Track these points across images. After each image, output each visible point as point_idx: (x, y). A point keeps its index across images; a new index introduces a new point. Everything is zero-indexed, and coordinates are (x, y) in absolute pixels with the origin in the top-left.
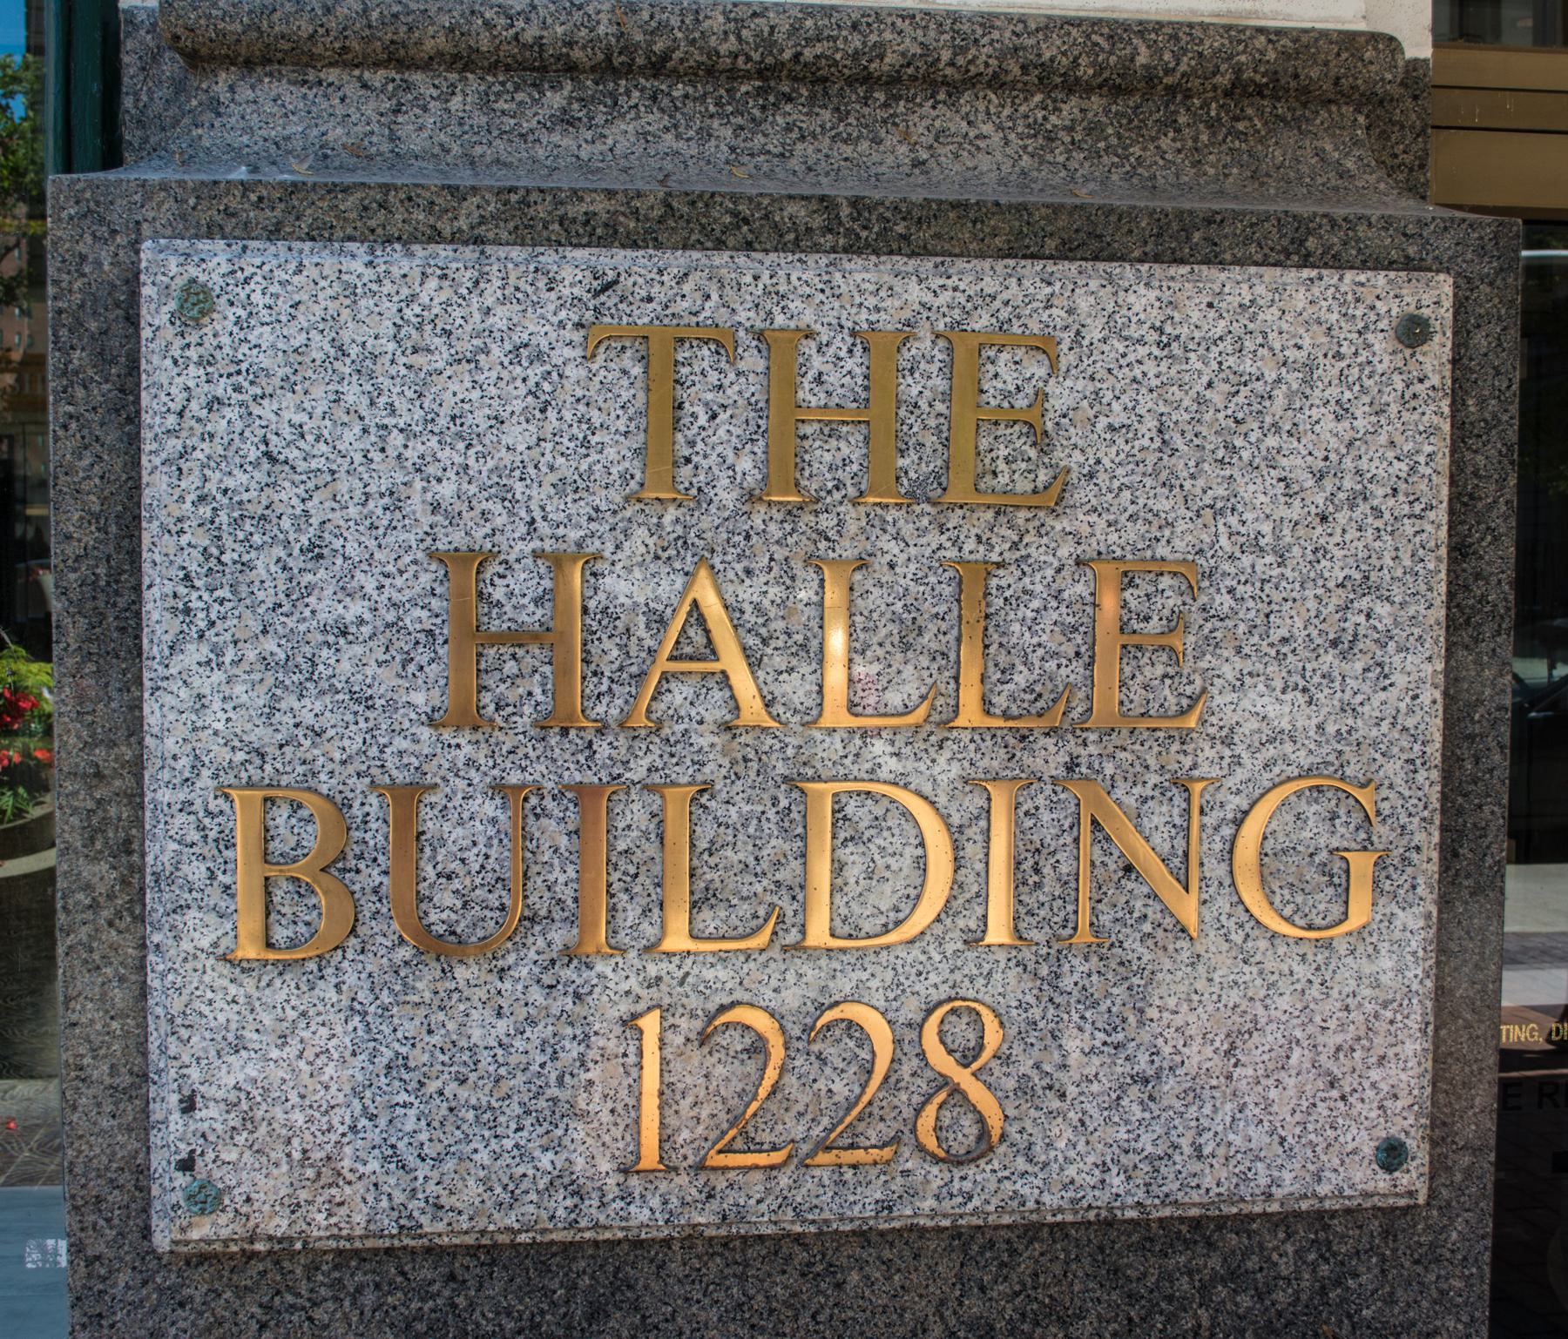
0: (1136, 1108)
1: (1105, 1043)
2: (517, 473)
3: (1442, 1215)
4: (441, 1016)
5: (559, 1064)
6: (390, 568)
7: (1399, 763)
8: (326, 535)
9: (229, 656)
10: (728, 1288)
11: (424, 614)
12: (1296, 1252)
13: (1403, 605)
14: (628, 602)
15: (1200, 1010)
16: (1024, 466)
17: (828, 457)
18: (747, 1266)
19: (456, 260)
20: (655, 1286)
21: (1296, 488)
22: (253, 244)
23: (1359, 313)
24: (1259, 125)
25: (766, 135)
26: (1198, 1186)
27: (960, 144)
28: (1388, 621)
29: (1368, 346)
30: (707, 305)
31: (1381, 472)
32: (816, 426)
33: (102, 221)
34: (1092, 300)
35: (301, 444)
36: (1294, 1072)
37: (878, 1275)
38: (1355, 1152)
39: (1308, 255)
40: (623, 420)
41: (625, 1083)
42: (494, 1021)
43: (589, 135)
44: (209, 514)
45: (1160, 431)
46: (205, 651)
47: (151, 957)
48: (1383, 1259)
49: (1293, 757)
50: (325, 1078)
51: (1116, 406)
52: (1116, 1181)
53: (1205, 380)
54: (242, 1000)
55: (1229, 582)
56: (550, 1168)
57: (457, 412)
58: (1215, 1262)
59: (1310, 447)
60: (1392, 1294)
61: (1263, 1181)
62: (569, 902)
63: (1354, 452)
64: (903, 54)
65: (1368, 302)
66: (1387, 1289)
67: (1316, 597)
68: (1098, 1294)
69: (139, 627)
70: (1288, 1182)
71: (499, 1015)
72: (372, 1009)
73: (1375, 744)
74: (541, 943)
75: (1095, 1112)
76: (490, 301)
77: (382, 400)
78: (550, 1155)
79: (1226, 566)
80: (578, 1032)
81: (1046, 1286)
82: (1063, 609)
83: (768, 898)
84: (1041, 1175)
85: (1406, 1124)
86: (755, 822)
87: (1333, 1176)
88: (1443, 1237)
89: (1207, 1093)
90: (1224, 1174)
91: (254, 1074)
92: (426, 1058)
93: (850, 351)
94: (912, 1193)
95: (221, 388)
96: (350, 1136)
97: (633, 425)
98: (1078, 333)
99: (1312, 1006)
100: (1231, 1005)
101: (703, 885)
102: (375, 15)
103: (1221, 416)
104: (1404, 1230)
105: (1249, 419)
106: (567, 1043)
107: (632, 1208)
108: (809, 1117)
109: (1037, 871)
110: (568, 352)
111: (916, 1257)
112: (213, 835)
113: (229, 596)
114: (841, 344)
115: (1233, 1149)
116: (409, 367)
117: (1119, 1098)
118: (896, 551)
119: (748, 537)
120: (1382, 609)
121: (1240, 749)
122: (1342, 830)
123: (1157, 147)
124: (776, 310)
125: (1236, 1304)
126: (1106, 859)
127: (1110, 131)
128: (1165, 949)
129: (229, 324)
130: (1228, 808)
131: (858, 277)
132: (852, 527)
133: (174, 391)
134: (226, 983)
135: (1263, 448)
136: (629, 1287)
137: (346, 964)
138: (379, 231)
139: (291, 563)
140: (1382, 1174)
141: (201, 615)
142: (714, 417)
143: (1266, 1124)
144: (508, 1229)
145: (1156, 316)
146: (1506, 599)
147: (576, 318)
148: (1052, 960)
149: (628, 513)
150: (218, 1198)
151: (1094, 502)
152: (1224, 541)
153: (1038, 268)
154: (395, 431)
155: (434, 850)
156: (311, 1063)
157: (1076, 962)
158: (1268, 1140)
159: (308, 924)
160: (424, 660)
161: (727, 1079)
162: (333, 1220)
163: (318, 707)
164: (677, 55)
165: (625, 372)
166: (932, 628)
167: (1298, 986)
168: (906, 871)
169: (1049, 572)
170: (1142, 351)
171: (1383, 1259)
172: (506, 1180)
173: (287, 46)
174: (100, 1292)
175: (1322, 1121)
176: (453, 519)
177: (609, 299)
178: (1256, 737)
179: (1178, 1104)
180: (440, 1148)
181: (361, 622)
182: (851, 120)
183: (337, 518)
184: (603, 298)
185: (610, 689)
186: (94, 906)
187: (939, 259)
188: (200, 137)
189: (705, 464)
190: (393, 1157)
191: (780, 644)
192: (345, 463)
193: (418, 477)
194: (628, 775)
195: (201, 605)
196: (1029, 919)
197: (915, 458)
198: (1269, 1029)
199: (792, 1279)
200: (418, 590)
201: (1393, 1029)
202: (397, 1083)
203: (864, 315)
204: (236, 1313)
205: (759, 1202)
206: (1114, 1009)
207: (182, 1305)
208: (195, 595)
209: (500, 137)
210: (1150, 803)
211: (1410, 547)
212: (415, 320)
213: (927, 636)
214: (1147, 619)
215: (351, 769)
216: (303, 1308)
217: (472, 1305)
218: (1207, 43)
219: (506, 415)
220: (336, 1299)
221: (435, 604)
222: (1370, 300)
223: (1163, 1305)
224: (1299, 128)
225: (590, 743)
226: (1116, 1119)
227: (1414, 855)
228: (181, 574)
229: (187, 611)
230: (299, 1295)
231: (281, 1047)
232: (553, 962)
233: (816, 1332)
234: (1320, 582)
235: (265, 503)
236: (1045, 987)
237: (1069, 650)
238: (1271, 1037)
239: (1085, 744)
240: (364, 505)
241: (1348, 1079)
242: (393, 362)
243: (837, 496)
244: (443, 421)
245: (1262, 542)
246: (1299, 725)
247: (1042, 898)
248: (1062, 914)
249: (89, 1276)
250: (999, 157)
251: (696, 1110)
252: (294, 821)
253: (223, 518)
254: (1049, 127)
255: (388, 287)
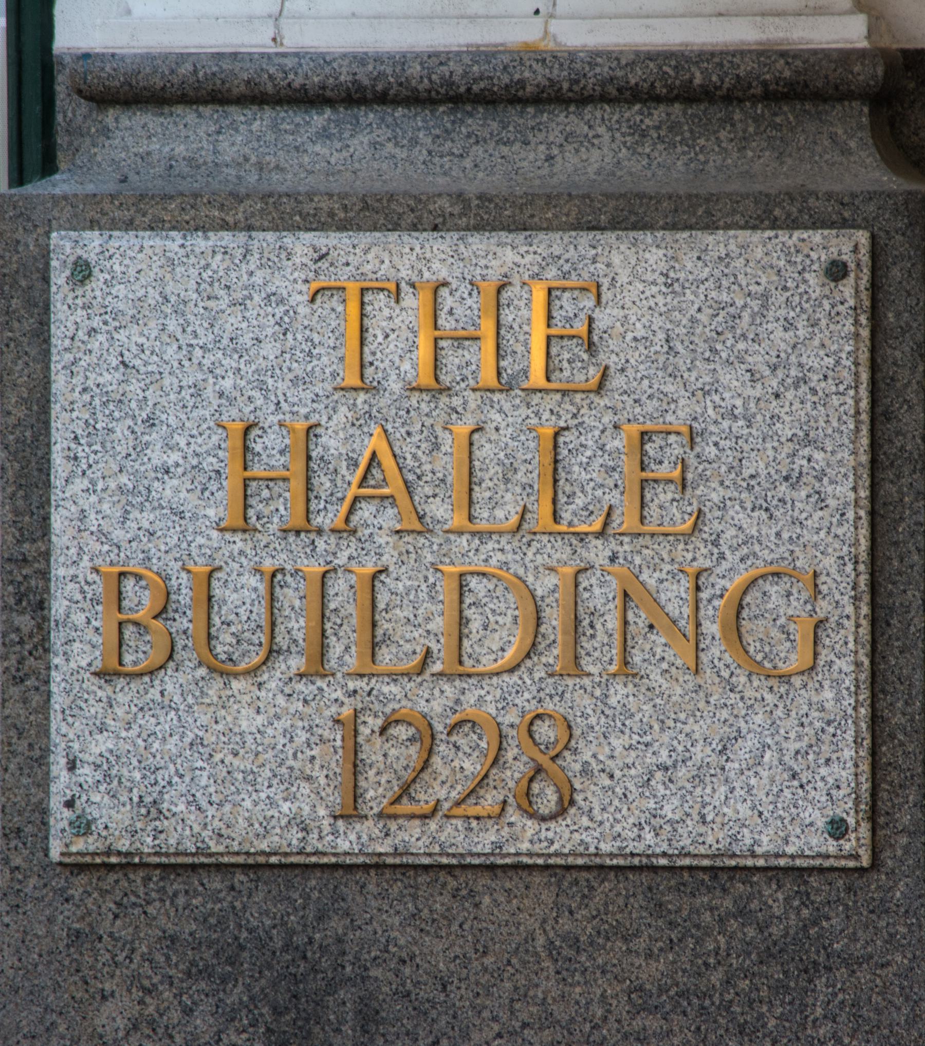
0: (661, 787)
1: (639, 743)
2: (269, 373)
3: (888, 879)
4: (223, 712)
5: (294, 745)
6: (195, 432)
7: (833, 559)
8: (157, 412)
9: (100, 486)
10: (406, 903)
11: (214, 460)
12: (785, 899)
13: (833, 453)
14: (336, 453)
15: (702, 722)
16: (580, 364)
17: (457, 361)
18: (418, 889)
19: (233, 242)
20: (359, 899)
21: (758, 376)
22: (116, 233)
23: (799, 260)
24: (791, 118)
25: (453, 141)
26: (704, 843)
27: (581, 142)
28: (823, 464)
29: (805, 281)
30: (383, 267)
31: (816, 365)
32: (450, 342)
33: (29, 219)
34: (622, 257)
35: (142, 356)
36: (767, 767)
37: (503, 899)
38: (811, 824)
39: (776, 219)
40: (333, 339)
41: (334, 759)
42: (255, 716)
43: (338, 145)
44: (89, 399)
45: (667, 341)
46: (86, 483)
47: (53, 673)
48: (847, 907)
49: (760, 554)
50: (153, 750)
51: (638, 325)
52: (649, 837)
53: (696, 306)
54: (104, 699)
55: (714, 438)
56: (288, 812)
57: (233, 336)
58: (728, 903)
59: (767, 349)
60: (854, 933)
61: (748, 841)
62: (301, 641)
63: (797, 352)
64: (538, 86)
65: (805, 252)
66: (851, 930)
67: (773, 448)
68: (649, 920)
69: (49, 468)
70: (765, 843)
71: (258, 712)
72: (182, 707)
73: (816, 545)
74: (283, 667)
75: (633, 789)
76: (252, 267)
77: (189, 329)
78: (288, 804)
79: (712, 428)
80: (306, 725)
81: (614, 914)
82: (606, 457)
83: (422, 641)
84: (598, 830)
85: (847, 807)
86: (413, 592)
87: (796, 840)
88: (890, 894)
89: (708, 779)
90: (721, 836)
91: (111, 747)
92: (213, 739)
93: (470, 294)
94: (515, 839)
95: (96, 322)
96: (168, 788)
97: (338, 343)
98: (613, 279)
99: (778, 722)
100: (722, 719)
101: (382, 632)
102: (201, 74)
103: (707, 330)
104: (861, 889)
105: (726, 332)
106: (299, 732)
107: (339, 840)
108: (448, 784)
109: (592, 626)
110: (299, 298)
111: (527, 888)
112: (89, 596)
113: (99, 449)
114: (464, 289)
115: (726, 819)
116: (205, 308)
117: (649, 780)
118: (500, 420)
119: (408, 412)
120: (818, 456)
121: (724, 548)
122: (795, 603)
123: (717, 138)
124: (424, 269)
125: (744, 934)
126: (637, 620)
127: (686, 128)
128: (677, 680)
129: (101, 284)
130: (717, 587)
131: (474, 247)
132: (472, 405)
133: (69, 324)
134: (95, 688)
135: (735, 350)
136: (343, 900)
137: (167, 678)
138: (192, 222)
139: (136, 429)
140: (831, 841)
141: (84, 461)
142: (387, 336)
143: (749, 802)
144: (263, 853)
145: (663, 266)
146: (919, 449)
147: (303, 277)
148: (603, 686)
149: (336, 397)
150: (89, 824)
151: (625, 387)
152: (710, 411)
153: (591, 237)
154: (197, 348)
155: (220, 607)
156: (145, 741)
157: (619, 687)
158: (750, 813)
159: (144, 652)
160: (214, 489)
161: (398, 758)
162: (157, 842)
163: (152, 517)
164: (392, 92)
165: (333, 310)
166: (523, 469)
167: (768, 709)
168: (508, 625)
169: (597, 433)
170: (654, 289)
171: (847, 907)
172: (261, 819)
173: (148, 94)
174: (18, 890)
175: (787, 802)
176: (232, 401)
177: (324, 264)
178: (735, 541)
179: (689, 786)
180: (221, 797)
181: (177, 465)
182: (511, 128)
183: (163, 401)
184: (320, 264)
185: (325, 508)
186: (21, 642)
187: (528, 233)
188: (95, 154)
189: (382, 366)
190: (193, 801)
191: (428, 479)
192: (168, 367)
193: (211, 375)
194: (336, 561)
195: (84, 454)
196: (587, 658)
197: (511, 360)
198: (749, 736)
199: (446, 899)
200: (210, 445)
201: (835, 740)
202: (196, 755)
203: (478, 271)
204: (100, 907)
205: (418, 839)
206: (645, 720)
207: (67, 900)
208: (80, 448)
209: (282, 149)
210: (665, 583)
211: (837, 414)
212: (208, 280)
213: (520, 474)
214: (661, 463)
215: (170, 556)
216: (141, 906)
217: (244, 908)
218: (742, 68)
219: (262, 337)
220: (162, 900)
221: (221, 454)
222: (806, 251)
223: (693, 931)
224: (820, 120)
225: (313, 541)
226: (647, 794)
227: (845, 622)
228: (72, 436)
229: (76, 458)
230: (139, 897)
231: (127, 730)
232: (291, 679)
233: (463, 936)
234: (776, 438)
235: (121, 392)
236: (599, 703)
237: (610, 482)
238: (751, 742)
239: (621, 543)
240: (179, 393)
241: (805, 773)
242: (196, 305)
243: (463, 385)
244: (225, 341)
245: (736, 412)
246: (763, 532)
247: (596, 645)
248: (609, 655)
249: (12, 879)
250: (606, 150)
251: (378, 777)
252: (137, 588)
253: (97, 402)
254: (644, 127)
255: (193, 260)
